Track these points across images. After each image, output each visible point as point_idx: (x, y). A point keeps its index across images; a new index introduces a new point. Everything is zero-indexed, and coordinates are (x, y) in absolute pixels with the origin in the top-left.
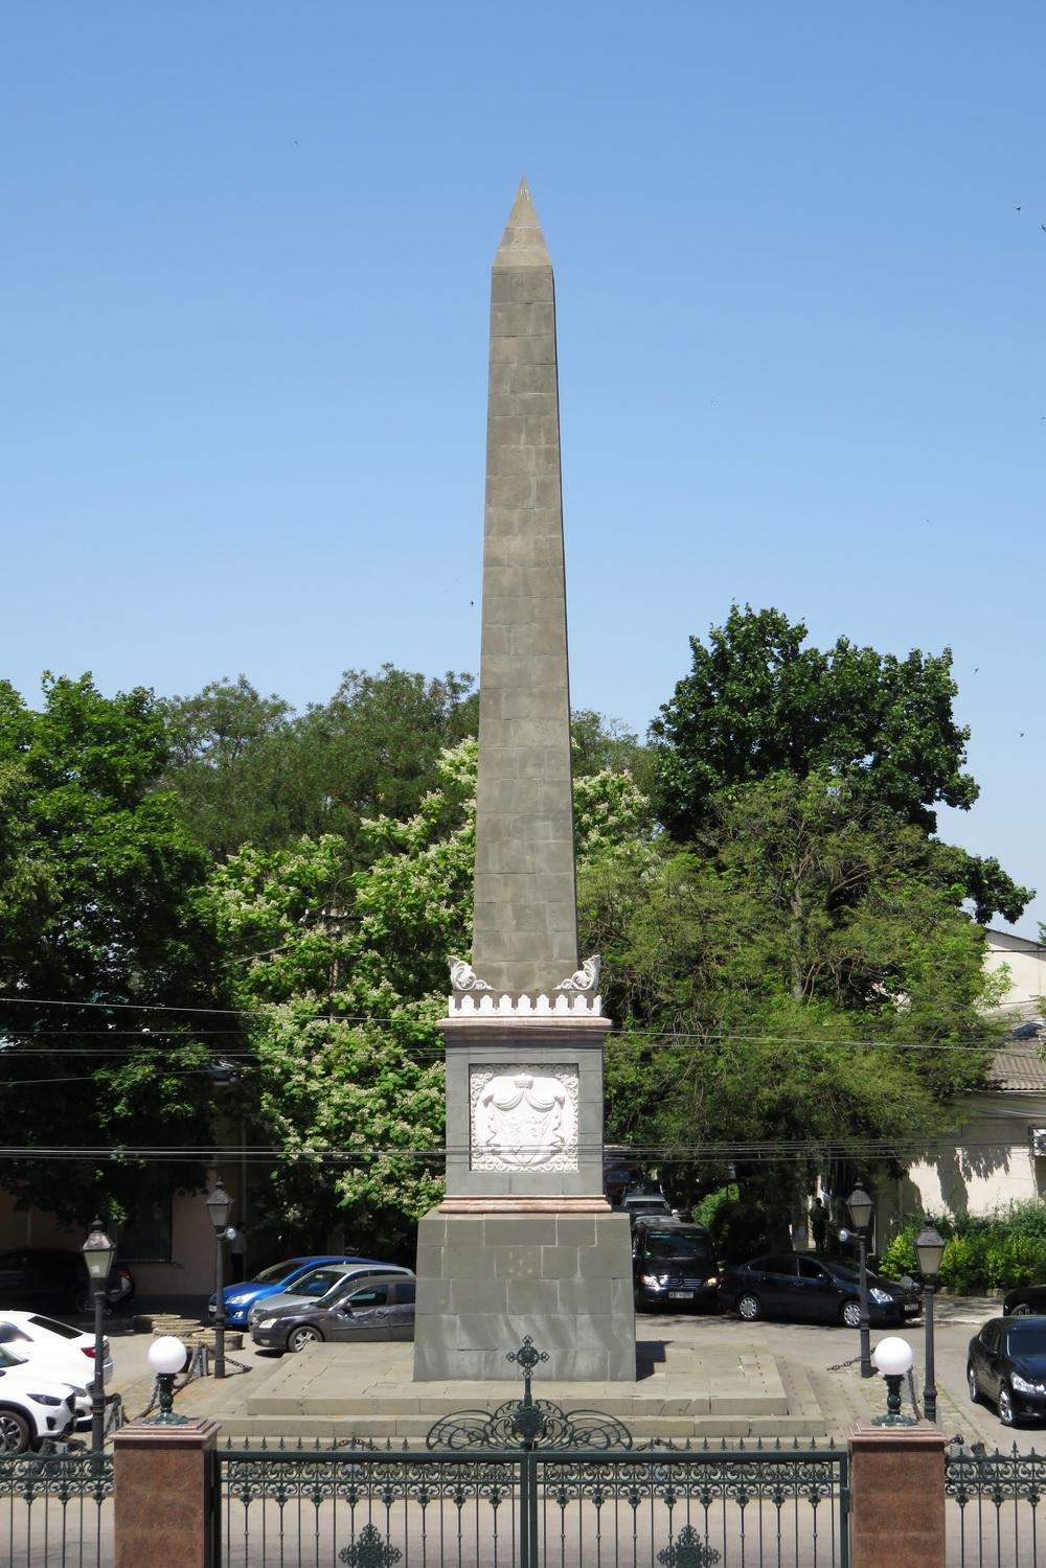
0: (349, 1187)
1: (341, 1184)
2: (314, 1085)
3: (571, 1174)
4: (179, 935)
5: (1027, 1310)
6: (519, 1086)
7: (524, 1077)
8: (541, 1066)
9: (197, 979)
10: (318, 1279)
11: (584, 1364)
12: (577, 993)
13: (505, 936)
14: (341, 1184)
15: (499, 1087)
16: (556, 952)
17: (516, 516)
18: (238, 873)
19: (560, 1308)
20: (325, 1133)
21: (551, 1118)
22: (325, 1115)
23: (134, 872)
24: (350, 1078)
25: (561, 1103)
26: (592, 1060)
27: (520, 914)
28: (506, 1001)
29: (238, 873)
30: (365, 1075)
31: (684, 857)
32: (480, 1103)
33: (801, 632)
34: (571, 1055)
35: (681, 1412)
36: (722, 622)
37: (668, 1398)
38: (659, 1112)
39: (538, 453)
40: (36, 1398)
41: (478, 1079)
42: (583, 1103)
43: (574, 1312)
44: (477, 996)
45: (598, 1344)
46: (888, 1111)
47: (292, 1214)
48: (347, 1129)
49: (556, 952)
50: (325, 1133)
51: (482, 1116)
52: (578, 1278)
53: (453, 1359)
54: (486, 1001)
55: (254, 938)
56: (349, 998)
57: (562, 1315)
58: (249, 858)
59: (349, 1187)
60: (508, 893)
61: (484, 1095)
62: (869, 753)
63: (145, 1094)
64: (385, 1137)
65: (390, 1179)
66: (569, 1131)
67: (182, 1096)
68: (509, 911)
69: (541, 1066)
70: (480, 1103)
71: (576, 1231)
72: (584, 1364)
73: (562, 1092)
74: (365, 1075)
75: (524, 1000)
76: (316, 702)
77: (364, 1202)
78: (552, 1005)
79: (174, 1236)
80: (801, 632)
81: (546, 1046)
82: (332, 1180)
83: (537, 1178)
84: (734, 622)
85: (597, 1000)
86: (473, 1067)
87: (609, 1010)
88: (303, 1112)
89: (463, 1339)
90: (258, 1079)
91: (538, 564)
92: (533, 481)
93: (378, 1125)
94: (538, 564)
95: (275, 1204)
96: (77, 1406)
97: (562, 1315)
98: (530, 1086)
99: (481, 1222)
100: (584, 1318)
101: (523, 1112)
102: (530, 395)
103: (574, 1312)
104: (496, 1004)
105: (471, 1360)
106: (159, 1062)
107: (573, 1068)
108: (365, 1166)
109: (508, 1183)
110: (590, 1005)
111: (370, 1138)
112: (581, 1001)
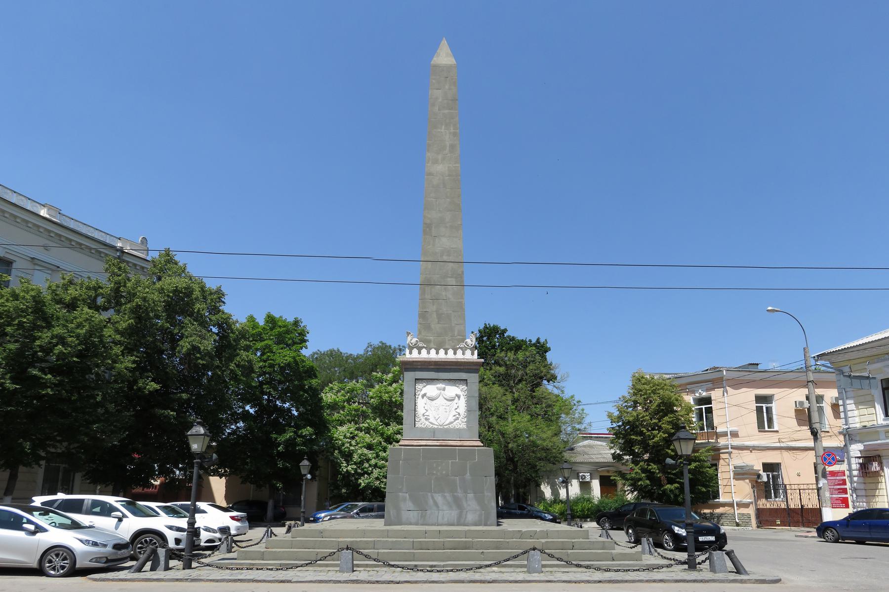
0: (363, 482)
1: (360, 481)
2: (352, 448)
3: (464, 429)
4: (305, 391)
5: (25, 520)
6: (439, 389)
7: (441, 385)
8: (450, 380)
9: (315, 415)
10: (686, 526)
11: (470, 517)
12: (466, 349)
13: (433, 326)
14: (360, 481)
15: (431, 390)
16: (456, 333)
17: (440, 157)
18: (332, 389)
19: (459, 490)
20: (355, 463)
21: (454, 404)
22: (356, 457)
23: (289, 365)
24: (364, 447)
25: (459, 397)
26: (474, 378)
27: (440, 317)
28: (433, 351)
29: (332, 389)
30: (370, 447)
31: (861, 480)
32: (420, 397)
33: (505, 331)
34: (463, 376)
35: (531, 537)
36: (482, 327)
37: (524, 530)
38: (306, 352)
39: (450, 133)
40: (170, 528)
41: (419, 386)
42: (469, 398)
43: (466, 492)
44: (419, 350)
45: (478, 508)
46: (623, 509)
47: (344, 491)
48: (361, 463)
49: (456, 333)
50: (355, 463)
51: (421, 403)
52: (468, 476)
53: (405, 515)
54: (424, 351)
55: (334, 407)
56: (366, 425)
57: (460, 494)
58: (336, 385)
59: (363, 482)
60: (434, 308)
61: (422, 392)
62: (646, 452)
63: (290, 443)
64: (376, 466)
65: (377, 479)
66: (462, 409)
67: (304, 444)
68: (435, 316)
69: (450, 380)
70: (420, 397)
71: (466, 453)
72: (470, 517)
73: (461, 393)
74: (370, 447)
75: (442, 352)
76: (226, 299)
77: (368, 486)
78: (455, 353)
79: (365, 520)
80: (505, 331)
81: (796, 524)
82: (357, 479)
83: (447, 431)
84: (486, 327)
85: (476, 352)
86: (417, 380)
87: (480, 355)
88: (348, 456)
89: (410, 505)
90: (332, 445)
91: (449, 175)
92: (448, 144)
93: (373, 462)
94: (449, 175)
95: (338, 488)
96: (539, 392)
97: (460, 494)
98: (444, 389)
99: (100, 494)
100: (471, 496)
101: (441, 401)
102: (446, 111)
103: (466, 492)
104: (429, 353)
105: (413, 515)
106: (295, 432)
107: (465, 381)
108: (369, 474)
109: (433, 432)
110: (473, 354)
111: (370, 466)
112: (468, 352)
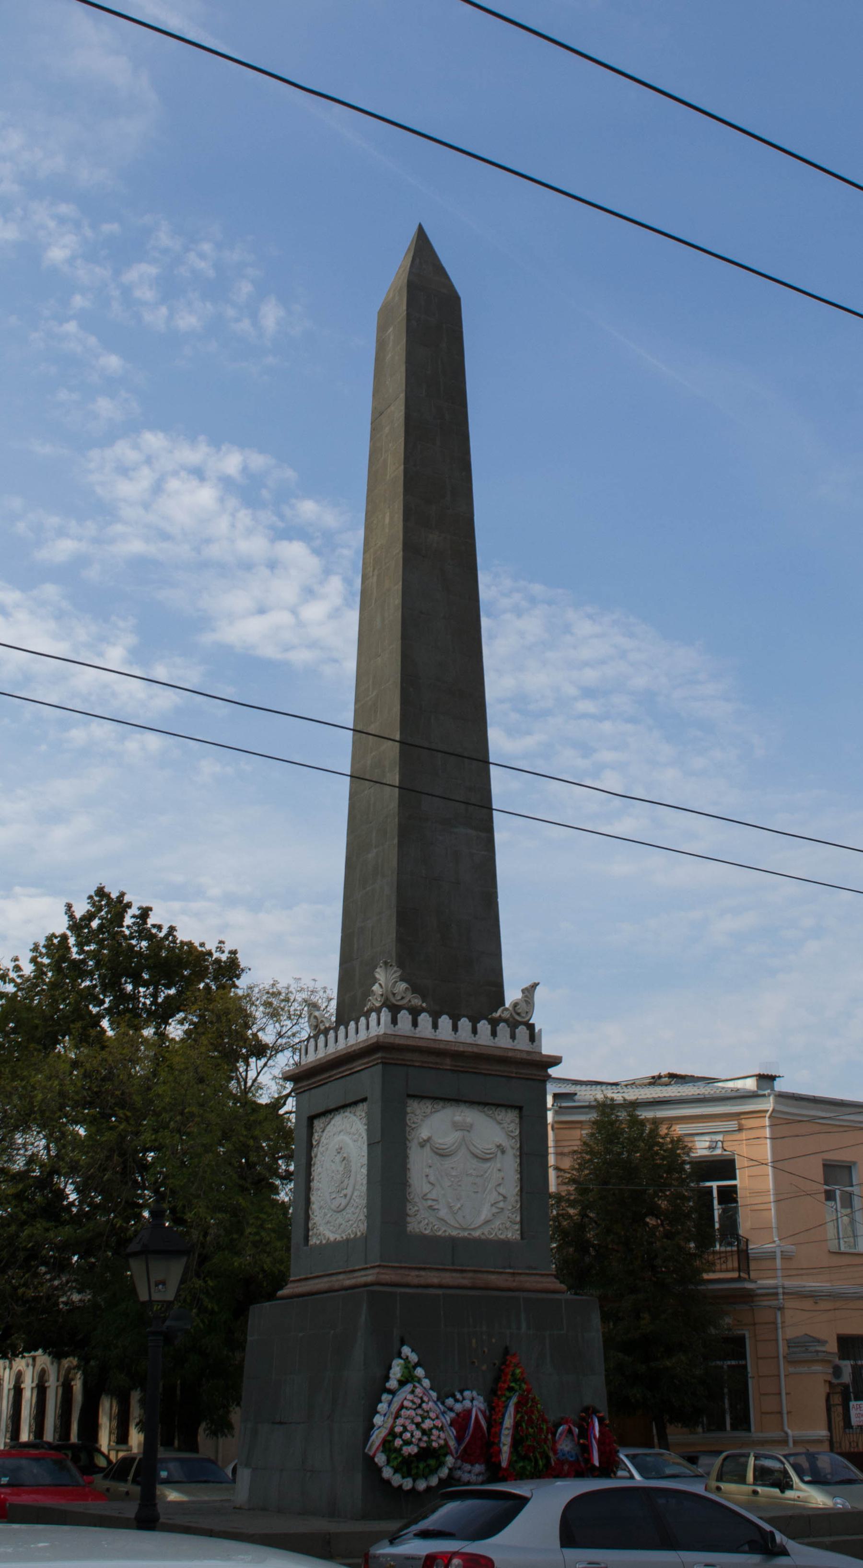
86: (410, 1096)
